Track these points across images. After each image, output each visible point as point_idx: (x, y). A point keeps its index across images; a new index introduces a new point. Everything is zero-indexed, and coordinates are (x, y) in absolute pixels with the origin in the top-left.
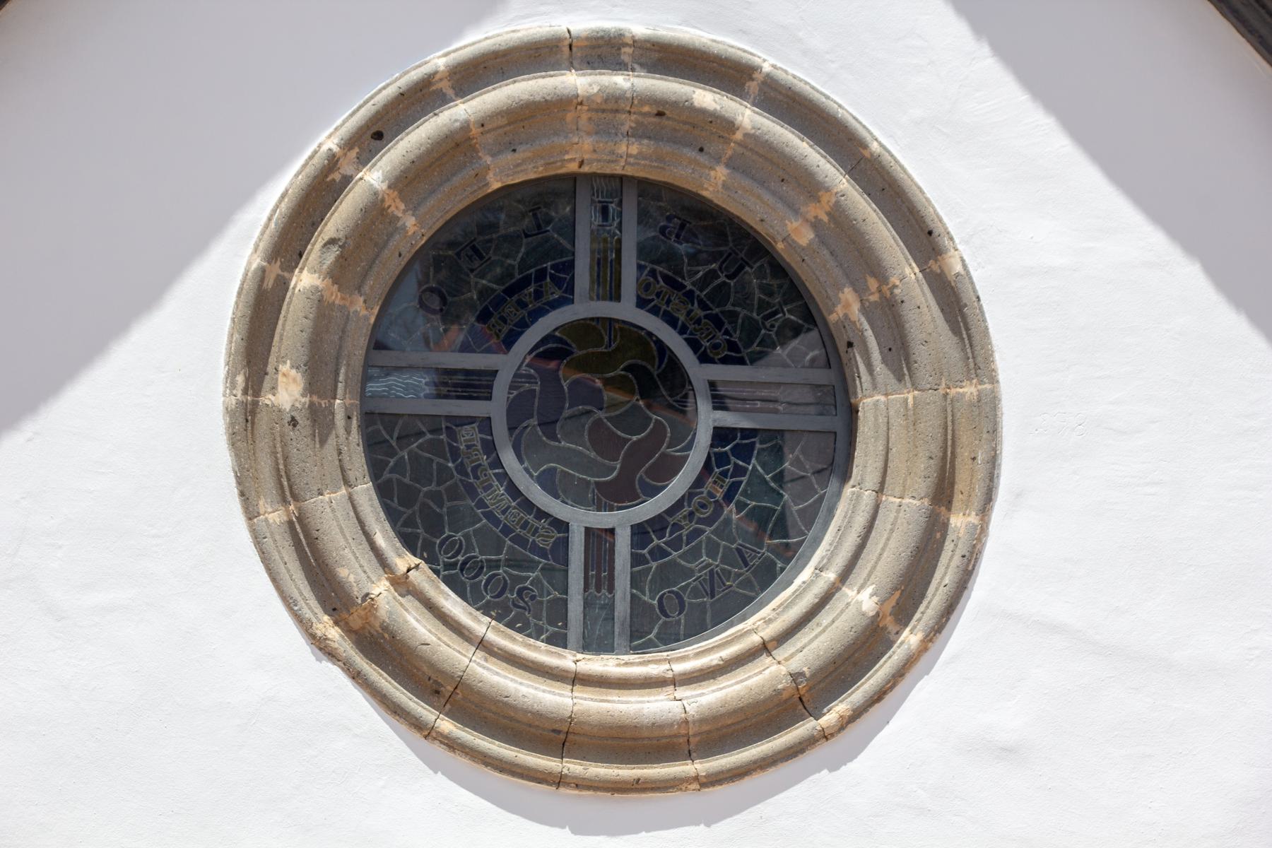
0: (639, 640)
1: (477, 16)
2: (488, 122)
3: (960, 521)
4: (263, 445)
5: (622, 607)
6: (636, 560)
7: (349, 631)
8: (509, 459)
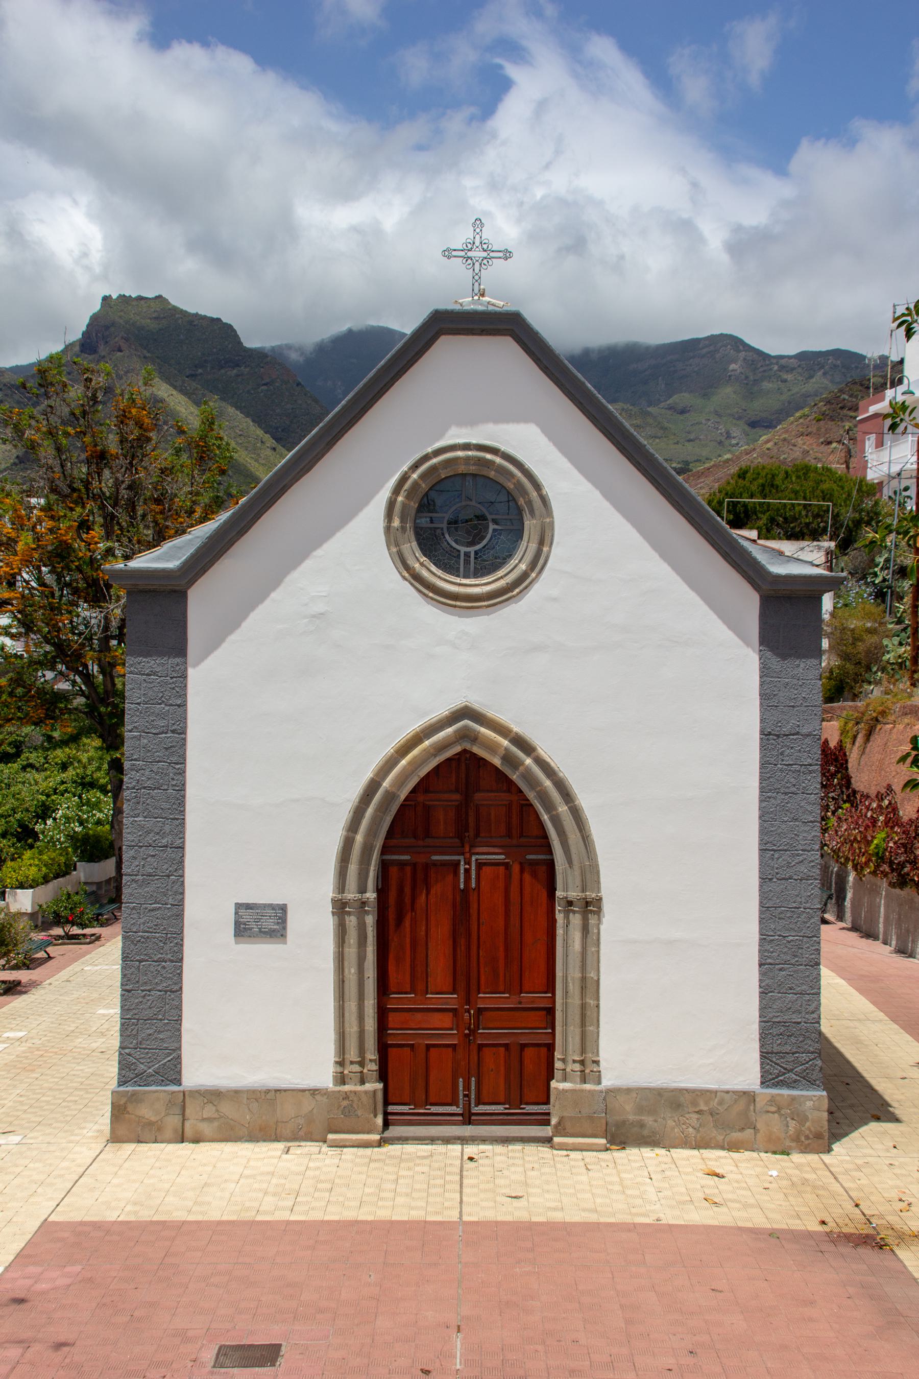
0: (476, 575)
1: (438, 440)
2: (440, 463)
3: (545, 549)
4: (392, 535)
5: (472, 569)
6: (476, 558)
7: (410, 575)
8: (447, 536)
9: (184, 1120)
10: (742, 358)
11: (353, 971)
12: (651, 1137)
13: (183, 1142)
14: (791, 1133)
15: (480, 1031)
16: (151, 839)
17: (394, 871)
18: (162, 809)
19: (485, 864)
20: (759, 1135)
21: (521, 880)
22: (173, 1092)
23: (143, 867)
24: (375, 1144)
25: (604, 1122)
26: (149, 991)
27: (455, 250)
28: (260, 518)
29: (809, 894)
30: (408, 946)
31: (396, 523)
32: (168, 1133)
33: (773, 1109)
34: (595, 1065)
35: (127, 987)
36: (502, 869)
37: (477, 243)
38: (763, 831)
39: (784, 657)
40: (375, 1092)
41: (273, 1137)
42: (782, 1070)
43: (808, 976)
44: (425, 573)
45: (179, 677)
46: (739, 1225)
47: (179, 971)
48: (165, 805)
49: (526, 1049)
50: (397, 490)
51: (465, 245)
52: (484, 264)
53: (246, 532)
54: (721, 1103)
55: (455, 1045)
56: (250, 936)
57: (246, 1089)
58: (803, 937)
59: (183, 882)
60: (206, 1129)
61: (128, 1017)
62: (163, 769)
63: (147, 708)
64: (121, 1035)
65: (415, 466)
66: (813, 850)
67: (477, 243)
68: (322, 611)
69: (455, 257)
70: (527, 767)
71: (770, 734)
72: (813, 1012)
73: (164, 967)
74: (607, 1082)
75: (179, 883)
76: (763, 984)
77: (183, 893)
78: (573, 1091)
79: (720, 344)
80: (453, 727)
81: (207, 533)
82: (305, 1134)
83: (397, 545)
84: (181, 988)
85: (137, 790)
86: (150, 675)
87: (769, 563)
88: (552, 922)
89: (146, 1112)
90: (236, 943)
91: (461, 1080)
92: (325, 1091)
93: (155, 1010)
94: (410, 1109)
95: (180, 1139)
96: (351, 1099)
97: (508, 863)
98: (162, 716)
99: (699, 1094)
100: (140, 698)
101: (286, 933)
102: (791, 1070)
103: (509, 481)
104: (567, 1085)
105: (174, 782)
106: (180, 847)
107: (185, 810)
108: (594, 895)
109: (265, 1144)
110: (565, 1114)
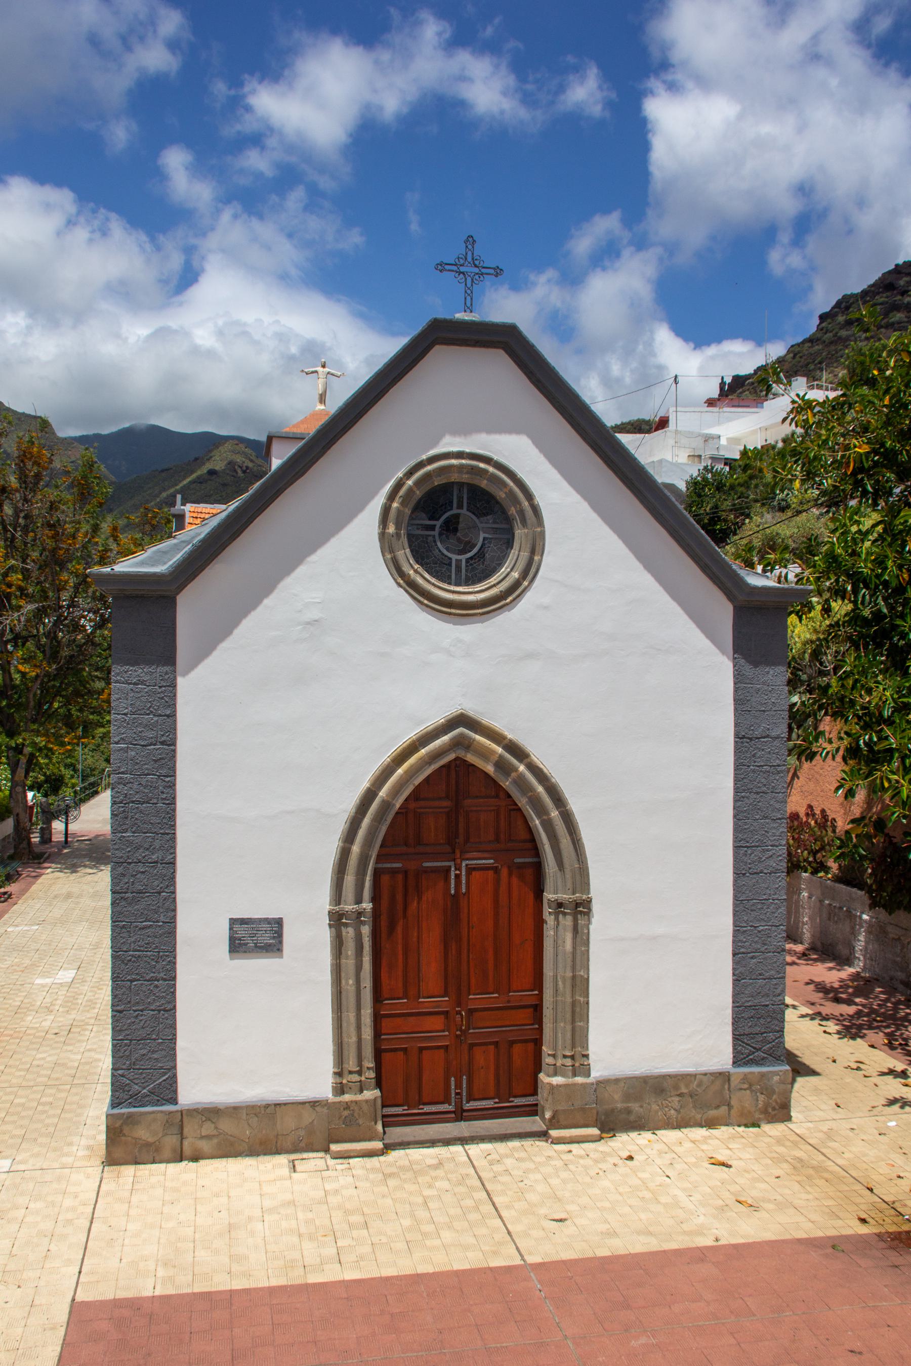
1: (432, 448)
3: (536, 558)
4: (386, 541)
5: (463, 576)
7: (405, 581)
8: (439, 544)
9: (182, 1139)
11: (351, 982)
12: (636, 1121)
13: (181, 1161)
14: (760, 1106)
15: (471, 1031)
16: (141, 855)
17: (385, 879)
18: (152, 823)
19: (474, 869)
20: (733, 1112)
21: (509, 883)
22: (171, 1112)
23: (132, 885)
24: (379, 1153)
28: (252, 522)
29: (777, 886)
30: (400, 952)
31: (391, 529)
32: (167, 1153)
33: (746, 1086)
34: (585, 1058)
35: (119, 1008)
36: (491, 873)
38: (737, 829)
39: (756, 664)
41: (274, 1150)
42: (752, 1050)
43: (775, 962)
44: (420, 580)
45: (168, 686)
47: (172, 990)
48: (154, 820)
49: (514, 1045)
50: (391, 497)
53: (239, 536)
54: (700, 1085)
55: (447, 1046)
56: (245, 952)
57: (244, 1105)
58: (772, 926)
59: (175, 898)
60: (205, 1146)
61: (120, 1038)
62: (152, 782)
64: (113, 1057)
65: (410, 473)
66: (781, 845)
68: (316, 617)
70: (521, 773)
71: (744, 737)
73: (157, 986)
74: (597, 1072)
75: (171, 900)
76: (737, 972)
77: (175, 910)
78: (566, 1086)
80: (449, 735)
82: (306, 1145)
83: (392, 551)
84: (175, 1007)
85: (125, 804)
86: (138, 684)
88: (539, 923)
89: (143, 1133)
90: (231, 959)
91: (453, 1079)
92: (325, 1102)
93: (149, 1030)
94: (404, 1110)
95: (179, 1158)
96: (351, 1108)
97: (497, 867)
98: (149, 726)
99: (680, 1078)
100: (126, 708)
101: (282, 946)
102: (760, 1049)
103: (502, 490)
104: (557, 1080)
105: (164, 796)
106: (171, 863)
107: (175, 824)
108: (584, 897)
110: (560, 1108)
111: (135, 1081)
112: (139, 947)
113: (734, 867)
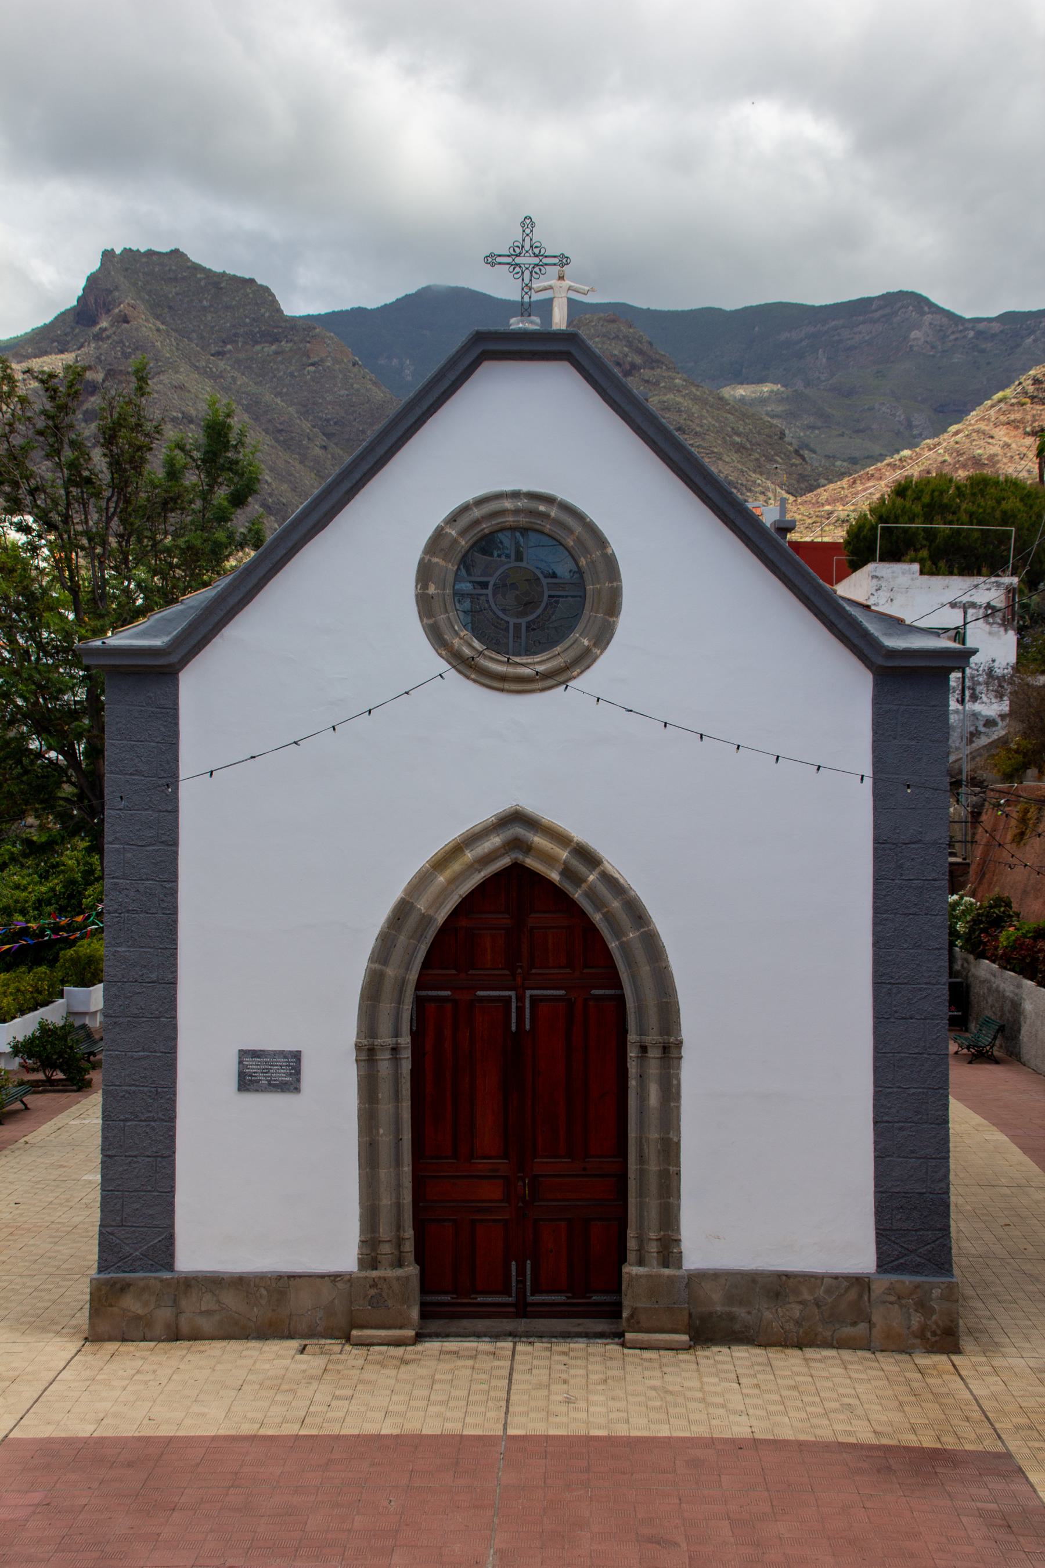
0: (528, 652)
10: (927, 323)
18: (150, 936)
20: (875, 1331)
24: (408, 1342)
25: (686, 1313)
26: (135, 1156)
27: (500, 256)
29: (934, 1037)
32: (159, 1329)
35: (110, 1153)
37: (527, 247)
40: (407, 1278)
41: (286, 1333)
46: (840, 1440)
51: (512, 249)
52: (536, 273)
54: (829, 1291)
56: (257, 1091)
61: (110, 1188)
63: (132, 815)
66: (939, 984)
67: (527, 247)
69: (500, 264)
72: (941, 1181)
73: (153, 1129)
78: (649, 1277)
79: (899, 305)
81: (202, 602)
87: (885, 634)
96: (379, 1286)
99: (802, 1280)
105: (165, 905)
106: (172, 983)
109: (276, 1342)
110: (639, 1305)
111: (125, 1241)
112: (134, 1080)
113: (874, 1009)
